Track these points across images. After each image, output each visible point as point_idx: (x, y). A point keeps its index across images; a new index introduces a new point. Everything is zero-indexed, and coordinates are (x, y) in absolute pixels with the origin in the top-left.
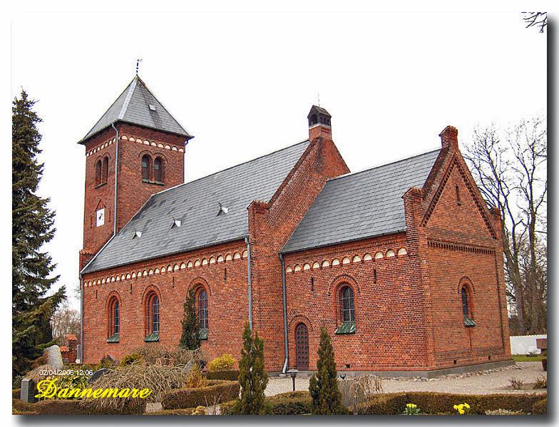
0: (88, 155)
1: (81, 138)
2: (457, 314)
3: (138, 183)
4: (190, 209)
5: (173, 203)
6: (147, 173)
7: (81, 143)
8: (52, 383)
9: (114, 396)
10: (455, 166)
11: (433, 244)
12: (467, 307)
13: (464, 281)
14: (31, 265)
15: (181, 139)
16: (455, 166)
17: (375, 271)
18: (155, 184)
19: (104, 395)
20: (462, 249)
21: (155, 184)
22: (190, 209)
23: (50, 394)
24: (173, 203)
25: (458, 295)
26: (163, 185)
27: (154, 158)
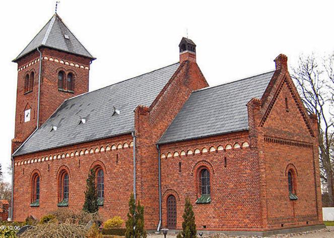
2: (285, 191)
3: (55, 91)
4: (93, 111)
5: (81, 106)
6: (61, 84)
11: (268, 140)
12: (292, 185)
16: (285, 83)
17: (225, 158)
18: (67, 92)
22: (93, 111)
24: (81, 106)
26: (73, 93)
27: (67, 73)
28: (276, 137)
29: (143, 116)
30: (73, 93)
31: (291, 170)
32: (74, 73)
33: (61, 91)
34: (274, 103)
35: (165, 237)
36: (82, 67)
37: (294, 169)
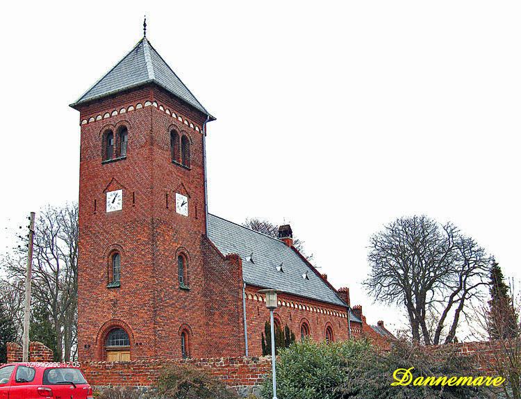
0: (85, 122)
1: (74, 101)
7: (75, 106)
8: (408, 371)
9: (443, 384)
15: (202, 117)
19: (458, 383)
23: (405, 383)
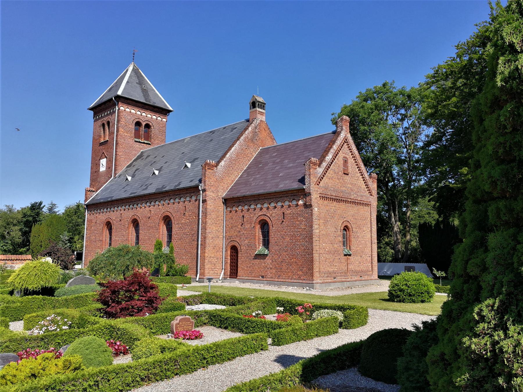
2: (338, 246)
3: (131, 141)
4: (166, 162)
5: (155, 157)
6: (137, 135)
10: (345, 144)
11: (324, 197)
12: (346, 241)
13: (345, 224)
14: (454, 83)
16: (345, 144)
17: (283, 213)
18: (144, 143)
20: (346, 201)
21: (144, 143)
22: (166, 162)
24: (155, 157)
25: (340, 233)
26: (150, 144)
27: (144, 124)
28: (332, 195)
29: (210, 170)
30: (150, 144)
31: (346, 226)
32: (151, 124)
33: (137, 142)
34: (332, 163)
35: (1, 260)
36: (159, 118)
37: (349, 225)
